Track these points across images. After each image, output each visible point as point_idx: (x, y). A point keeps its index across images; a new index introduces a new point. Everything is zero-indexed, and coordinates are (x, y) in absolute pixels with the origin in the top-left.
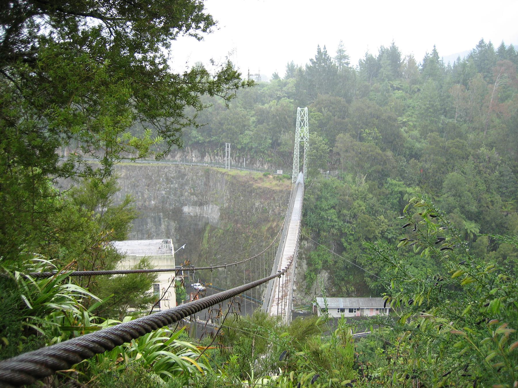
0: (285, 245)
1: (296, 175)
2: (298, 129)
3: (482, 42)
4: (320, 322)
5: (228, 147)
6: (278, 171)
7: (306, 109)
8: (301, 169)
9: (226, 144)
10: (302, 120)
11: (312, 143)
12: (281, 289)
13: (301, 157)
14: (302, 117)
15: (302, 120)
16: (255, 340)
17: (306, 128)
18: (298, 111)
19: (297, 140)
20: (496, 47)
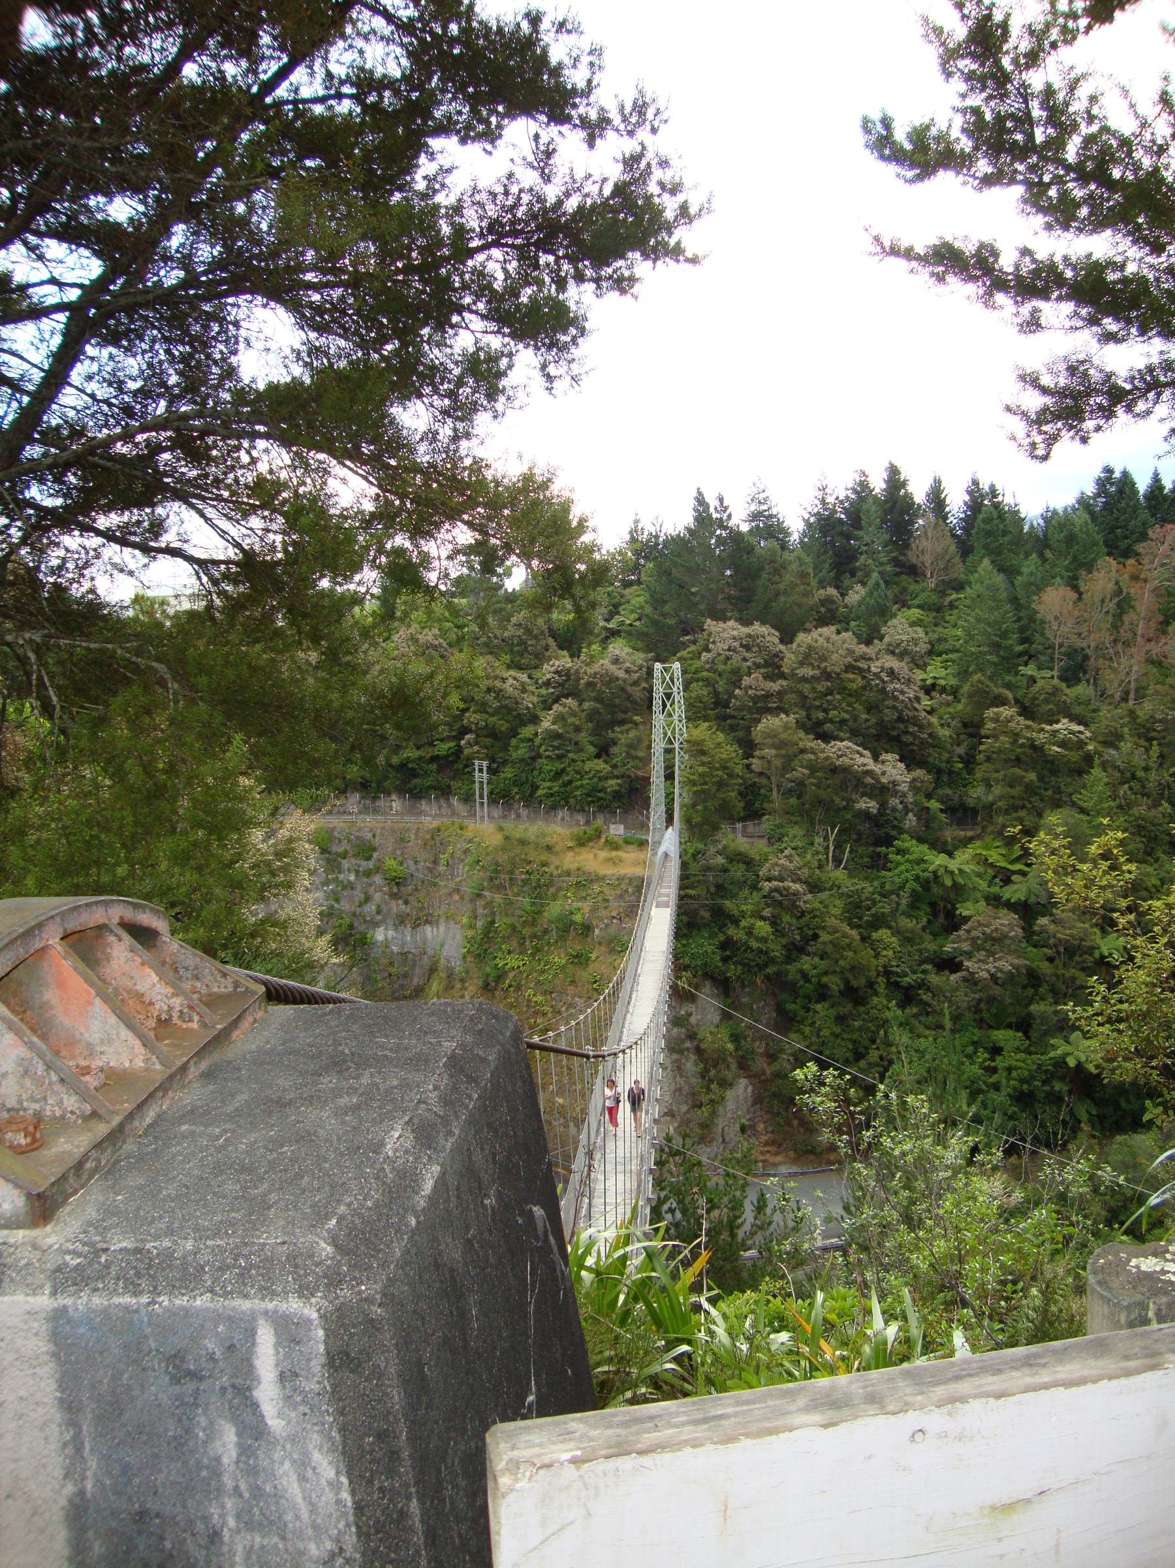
0: (678, 1446)
1: (657, 838)
2: (659, 719)
3: (1109, 471)
4: (1018, 957)
5: (481, 770)
6: (612, 826)
7: (677, 666)
8: (670, 820)
9: (477, 762)
10: (668, 696)
11: (697, 749)
12: (620, 1168)
13: (669, 777)
14: (670, 742)
15: (668, 696)
16: (882, 1298)
17: (679, 709)
18: (657, 674)
19: (658, 746)
20: (1142, 485)
